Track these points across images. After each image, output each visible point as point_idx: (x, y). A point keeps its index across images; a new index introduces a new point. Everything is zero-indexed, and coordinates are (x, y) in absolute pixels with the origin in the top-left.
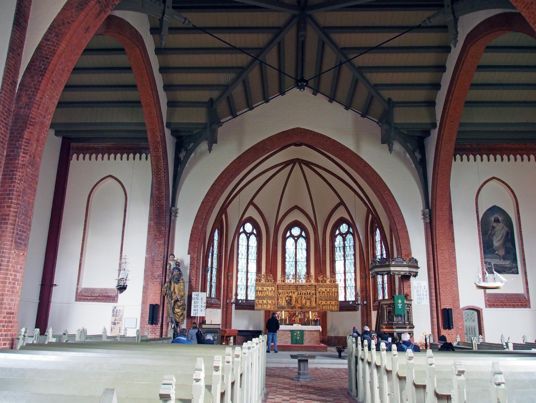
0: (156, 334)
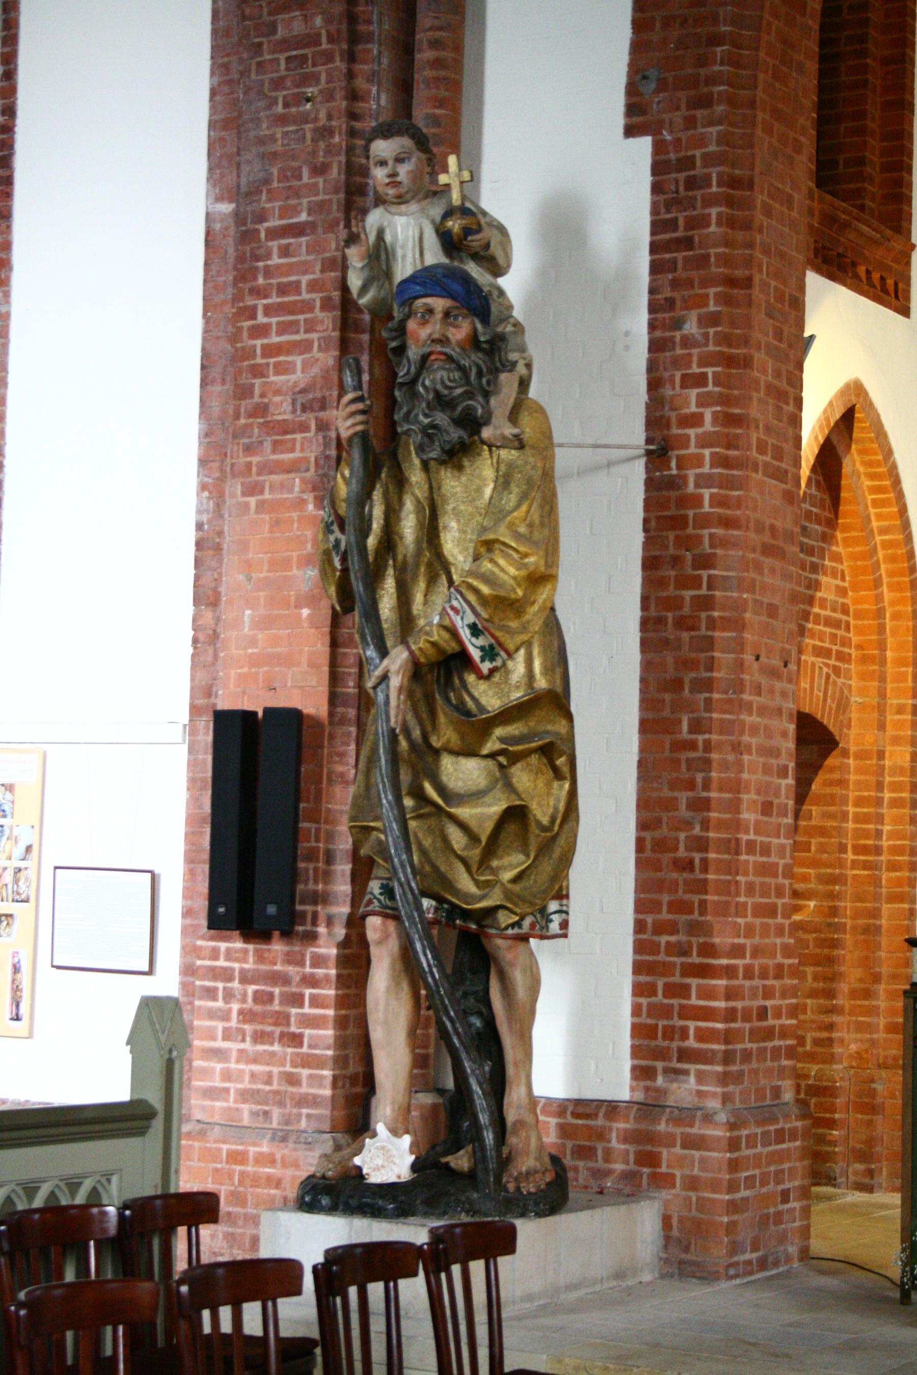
0: (296, 1040)
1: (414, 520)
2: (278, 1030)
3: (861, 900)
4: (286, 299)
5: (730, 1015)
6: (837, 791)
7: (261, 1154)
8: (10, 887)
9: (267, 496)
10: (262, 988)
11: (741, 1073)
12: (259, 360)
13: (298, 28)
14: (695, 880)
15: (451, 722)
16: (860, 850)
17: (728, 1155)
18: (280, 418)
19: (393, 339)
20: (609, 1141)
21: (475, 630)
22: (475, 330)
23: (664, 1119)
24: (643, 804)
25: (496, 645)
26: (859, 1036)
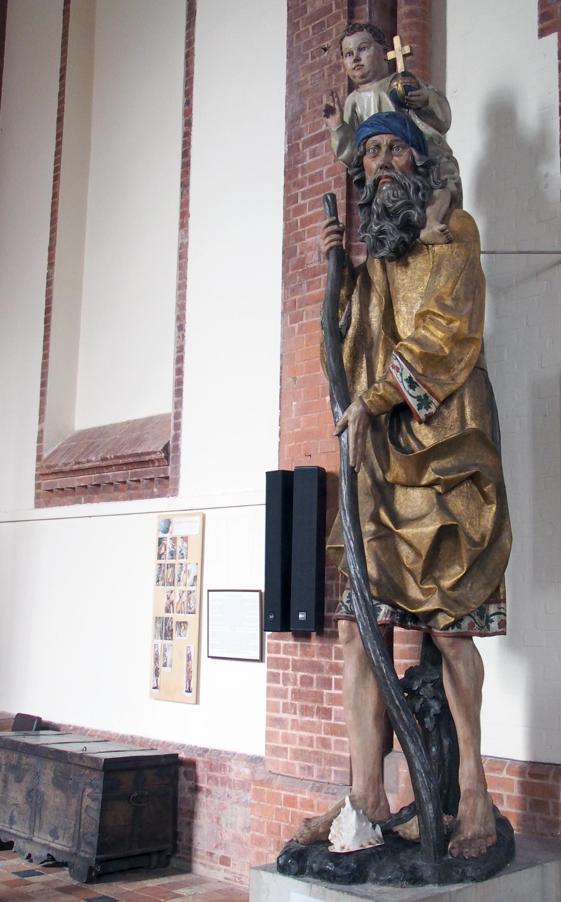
0: (327, 713)
1: (378, 311)
2: (316, 706)
8: (186, 603)
9: (305, 321)
10: (306, 674)
12: (299, 230)
15: (397, 459)
18: (311, 266)
19: (356, 174)
21: (412, 384)
22: (413, 158)
25: (428, 395)
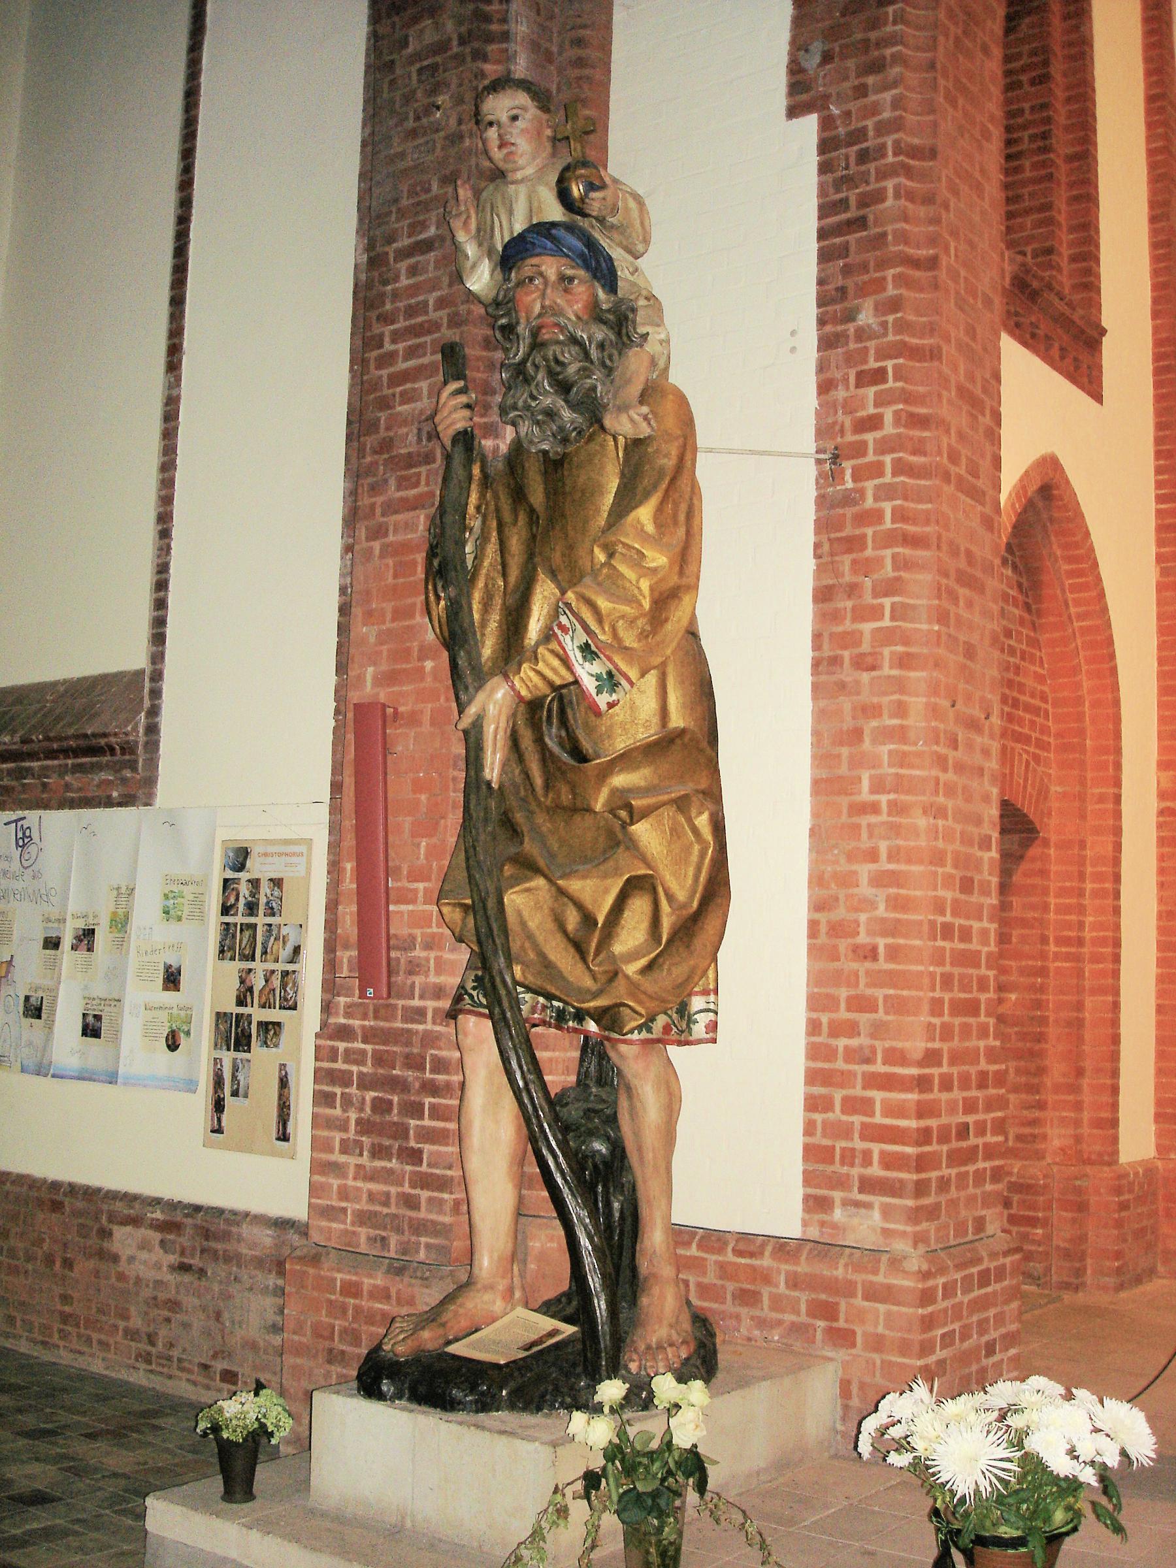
0: (415, 1156)
3: (1062, 993)
4: (413, 322)
5: (924, 1136)
6: (1037, 881)
7: (375, 1286)
9: (391, 538)
11: (937, 1206)
13: (430, 37)
14: (880, 971)
16: (1061, 941)
17: (920, 1311)
20: (777, 1286)
23: (842, 1262)
24: (817, 880)
26: (1063, 1131)
